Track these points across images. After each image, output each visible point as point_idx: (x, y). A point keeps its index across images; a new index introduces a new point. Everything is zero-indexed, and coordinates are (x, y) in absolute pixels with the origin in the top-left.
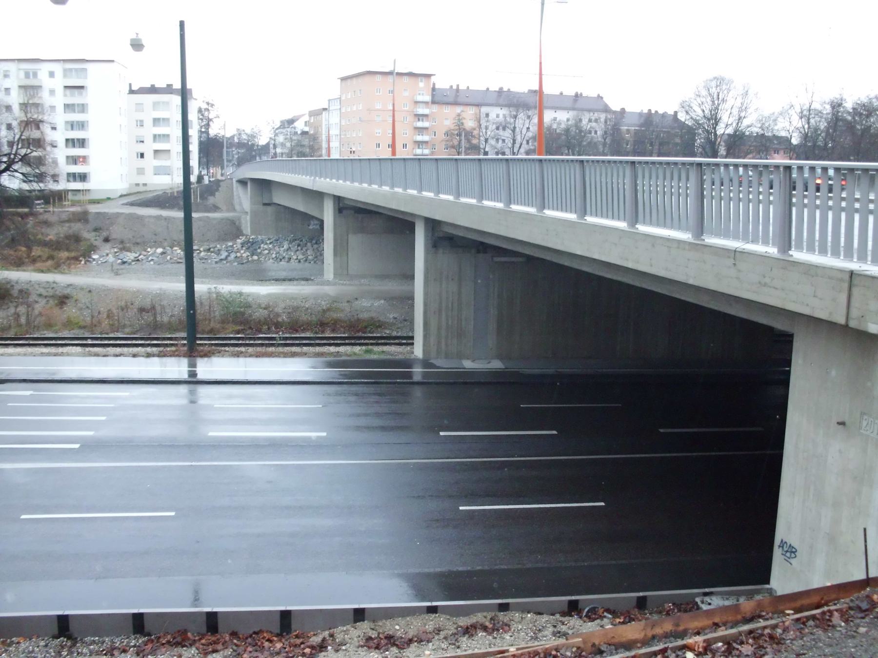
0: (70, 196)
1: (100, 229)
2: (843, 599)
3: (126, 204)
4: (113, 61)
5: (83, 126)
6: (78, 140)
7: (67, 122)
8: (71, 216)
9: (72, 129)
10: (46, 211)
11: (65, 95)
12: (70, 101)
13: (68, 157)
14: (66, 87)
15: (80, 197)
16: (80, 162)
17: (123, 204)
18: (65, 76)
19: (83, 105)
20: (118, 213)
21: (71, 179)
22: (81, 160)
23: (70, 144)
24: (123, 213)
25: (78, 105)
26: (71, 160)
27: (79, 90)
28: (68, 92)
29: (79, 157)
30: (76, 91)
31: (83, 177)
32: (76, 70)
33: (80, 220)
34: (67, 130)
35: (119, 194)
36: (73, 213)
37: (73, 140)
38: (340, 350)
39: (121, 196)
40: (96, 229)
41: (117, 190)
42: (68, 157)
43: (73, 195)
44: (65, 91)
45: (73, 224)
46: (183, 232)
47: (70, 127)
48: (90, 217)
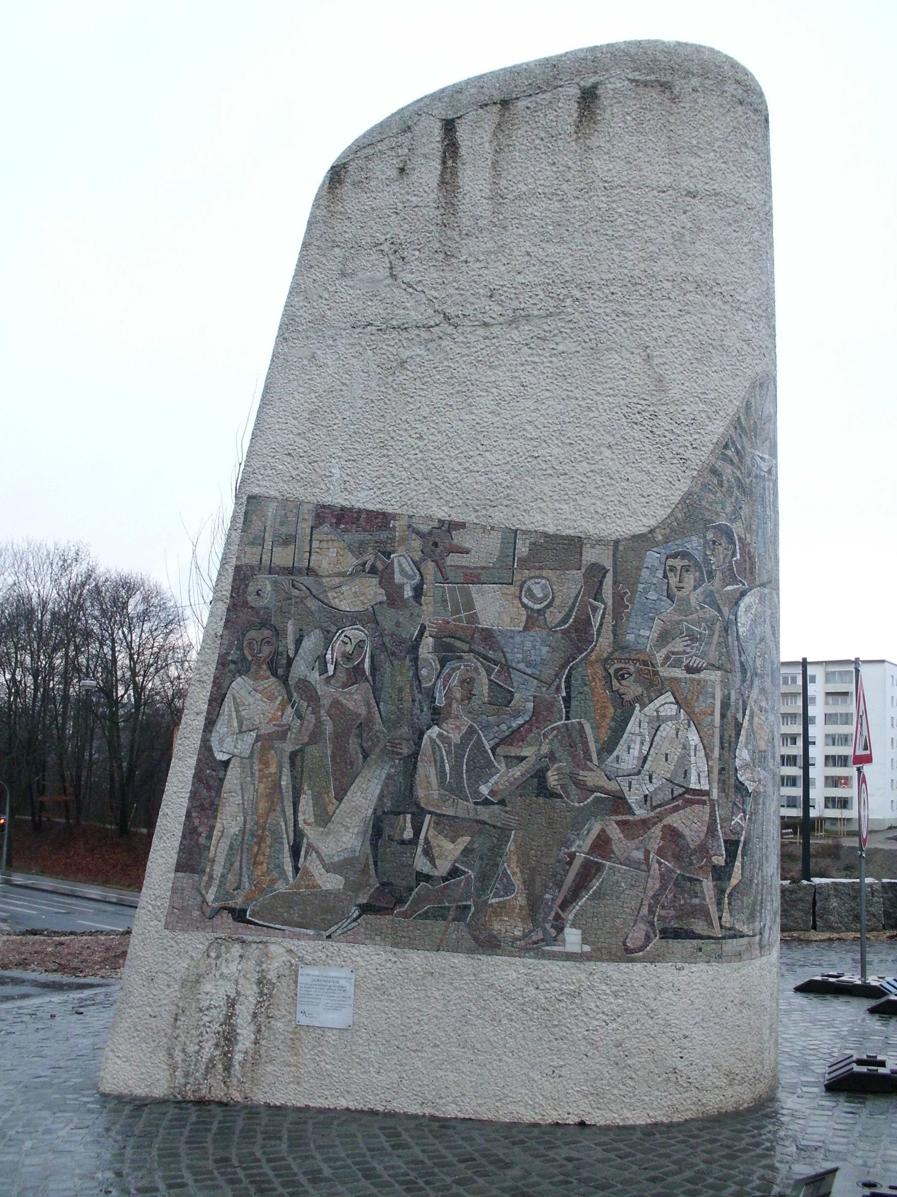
0: (827, 826)
1: (852, 868)
2: (74, 724)
3: (891, 839)
4: (883, 661)
5: (846, 740)
6: (840, 757)
7: (827, 736)
8: (820, 850)
9: (834, 744)
10: (792, 843)
11: (827, 703)
12: (832, 710)
13: (827, 778)
14: (828, 694)
15: (839, 827)
16: (841, 784)
17: (888, 838)
18: (827, 680)
19: (847, 714)
20: (876, 848)
21: (830, 805)
22: (843, 781)
23: (831, 761)
24: (881, 850)
25: (841, 714)
26: (830, 781)
27: (843, 697)
28: (830, 699)
29: (840, 778)
30: (840, 698)
31: (844, 803)
32: (840, 673)
33: (829, 855)
34: (827, 745)
35: (888, 825)
36: (823, 846)
37: (834, 757)
38: (234, 828)
39: (890, 828)
40: (848, 867)
41: (884, 820)
42: (827, 778)
43: (832, 824)
44: (826, 697)
45: (819, 860)
46: (152, 850)
47: (830, 742)
48: (842, 853)
